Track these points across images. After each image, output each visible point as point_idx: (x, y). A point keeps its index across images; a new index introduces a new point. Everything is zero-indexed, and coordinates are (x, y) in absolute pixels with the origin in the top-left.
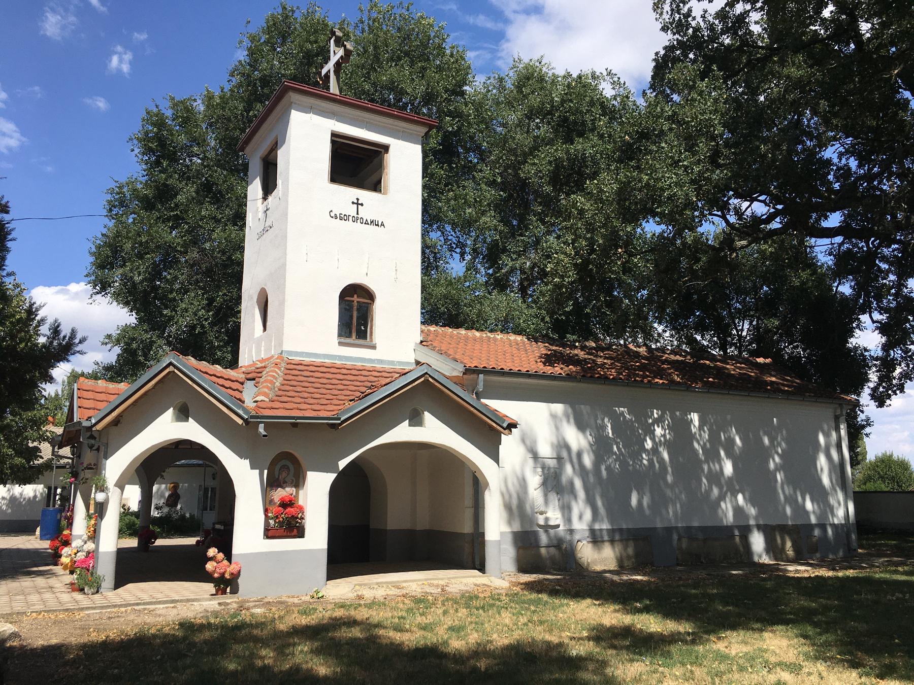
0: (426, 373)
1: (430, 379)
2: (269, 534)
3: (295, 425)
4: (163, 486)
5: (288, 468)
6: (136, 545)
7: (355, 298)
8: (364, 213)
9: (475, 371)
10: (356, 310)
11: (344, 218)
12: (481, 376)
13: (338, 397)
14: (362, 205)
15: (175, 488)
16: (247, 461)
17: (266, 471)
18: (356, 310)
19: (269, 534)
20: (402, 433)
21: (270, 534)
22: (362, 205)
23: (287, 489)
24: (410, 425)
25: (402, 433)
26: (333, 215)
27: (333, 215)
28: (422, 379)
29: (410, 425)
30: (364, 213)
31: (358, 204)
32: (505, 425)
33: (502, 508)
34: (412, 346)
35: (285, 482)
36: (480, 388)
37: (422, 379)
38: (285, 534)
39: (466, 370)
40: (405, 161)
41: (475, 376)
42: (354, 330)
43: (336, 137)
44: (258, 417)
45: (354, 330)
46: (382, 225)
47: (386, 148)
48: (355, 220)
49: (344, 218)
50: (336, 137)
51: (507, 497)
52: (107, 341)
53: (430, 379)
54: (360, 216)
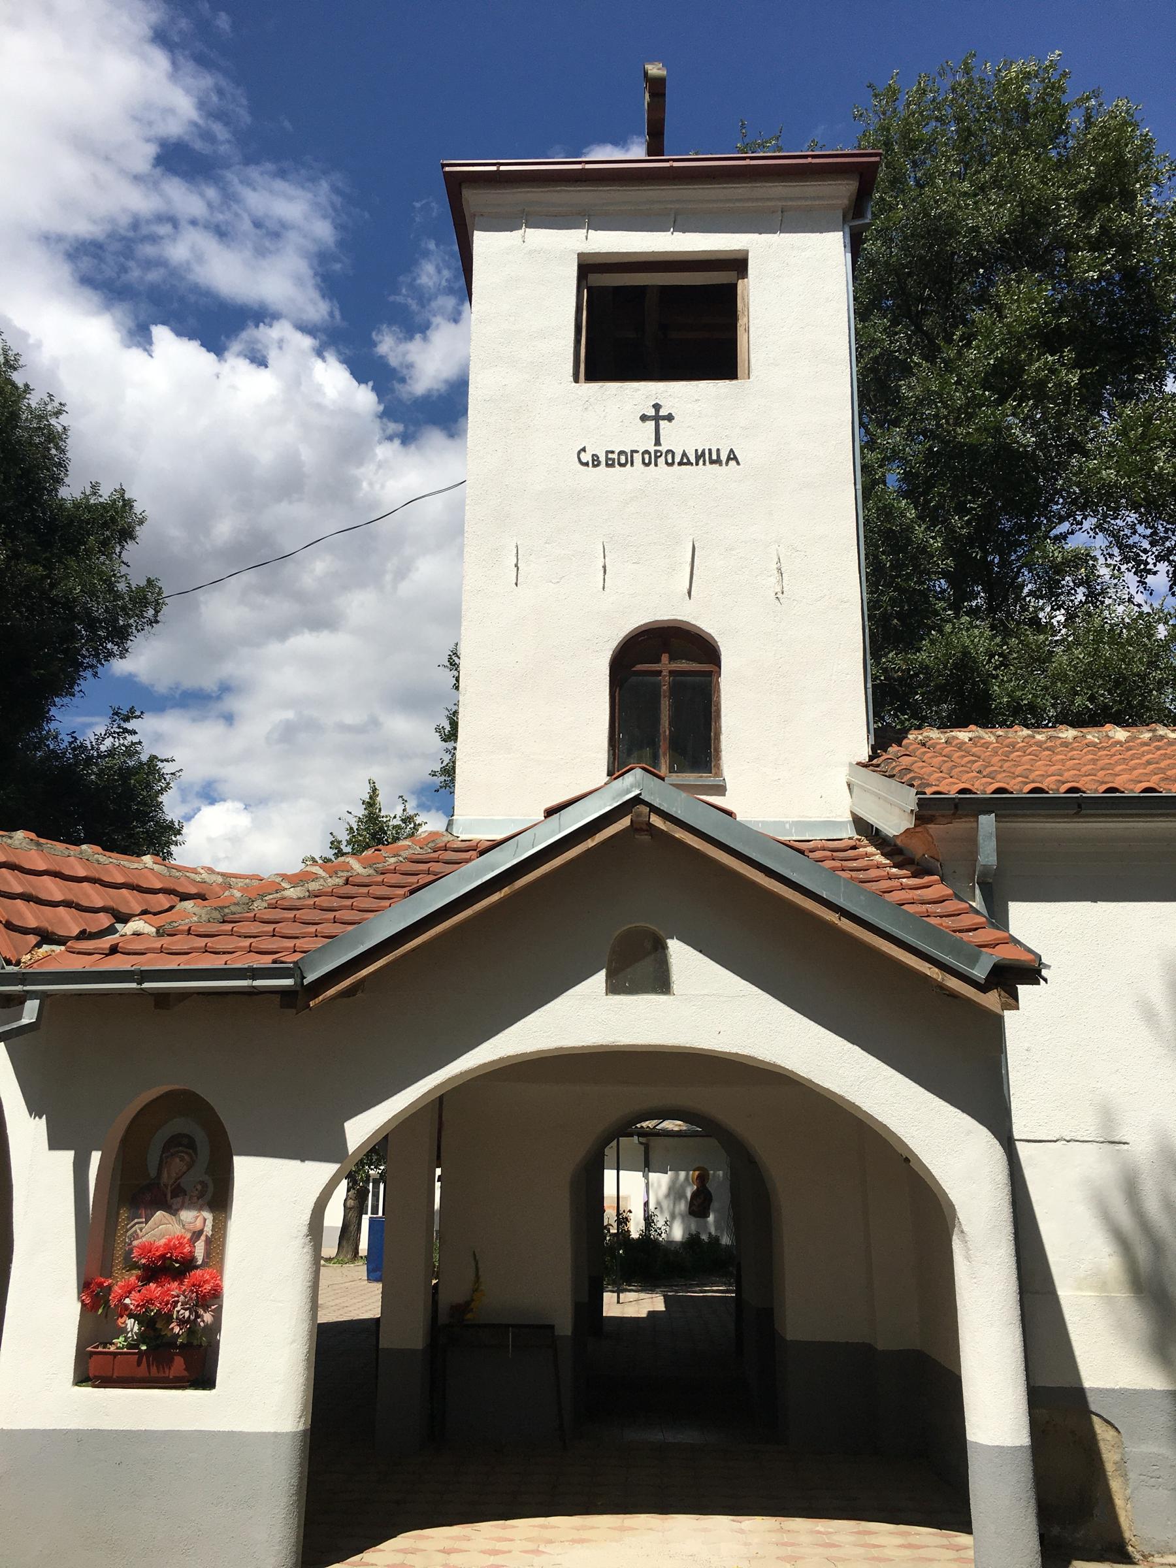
0: (637, 800)
1: (656, 820)
2: (93, 1368)
3: (162, 999)
4: (682, 1174)
5: (191, 1145)
6: (609, 1298)
7: (666, 664)
8: (675, 438)
9: (966, 806)
10: (665, 690)
11: (618, 460)
12: (987, 822)
13: (356, 902)
14: (670, 418)
15: (702, 1179)
16: (42, 1123)
17: (96, 1157)
18: (665, 690)
19: (93, 1368)
20: (585, 1016)
21: (93, 1368)
22: (670, 418)
23: (187, 1215)
24: (613, 988)
25: (585, 1016)
26: (586, 457)
27: (586, 457)
28: (625, 822)
29: (613, 988)
30: (675, 438)
31: (657, 418)
32: (980, 972)
33: (1122, 1295)
34: (841, 776)
35: (178, 1191)
36: (988, 855)
37: (625, 822)
38: (142, 1371)
39: (922, 803)
40: (800, 292)
41: (959, 826)
42: (664, 746)
43: (588, 267)
44: (24, 978)
45: (664, 746)
46: (732, 457)
47: (738, 264)
48: (650, 458)
49: (618, 460)
50: (588, 267)
51: (1142, 1253)
52: (320, 862)
53: (656, 820)
54: (663, 448)
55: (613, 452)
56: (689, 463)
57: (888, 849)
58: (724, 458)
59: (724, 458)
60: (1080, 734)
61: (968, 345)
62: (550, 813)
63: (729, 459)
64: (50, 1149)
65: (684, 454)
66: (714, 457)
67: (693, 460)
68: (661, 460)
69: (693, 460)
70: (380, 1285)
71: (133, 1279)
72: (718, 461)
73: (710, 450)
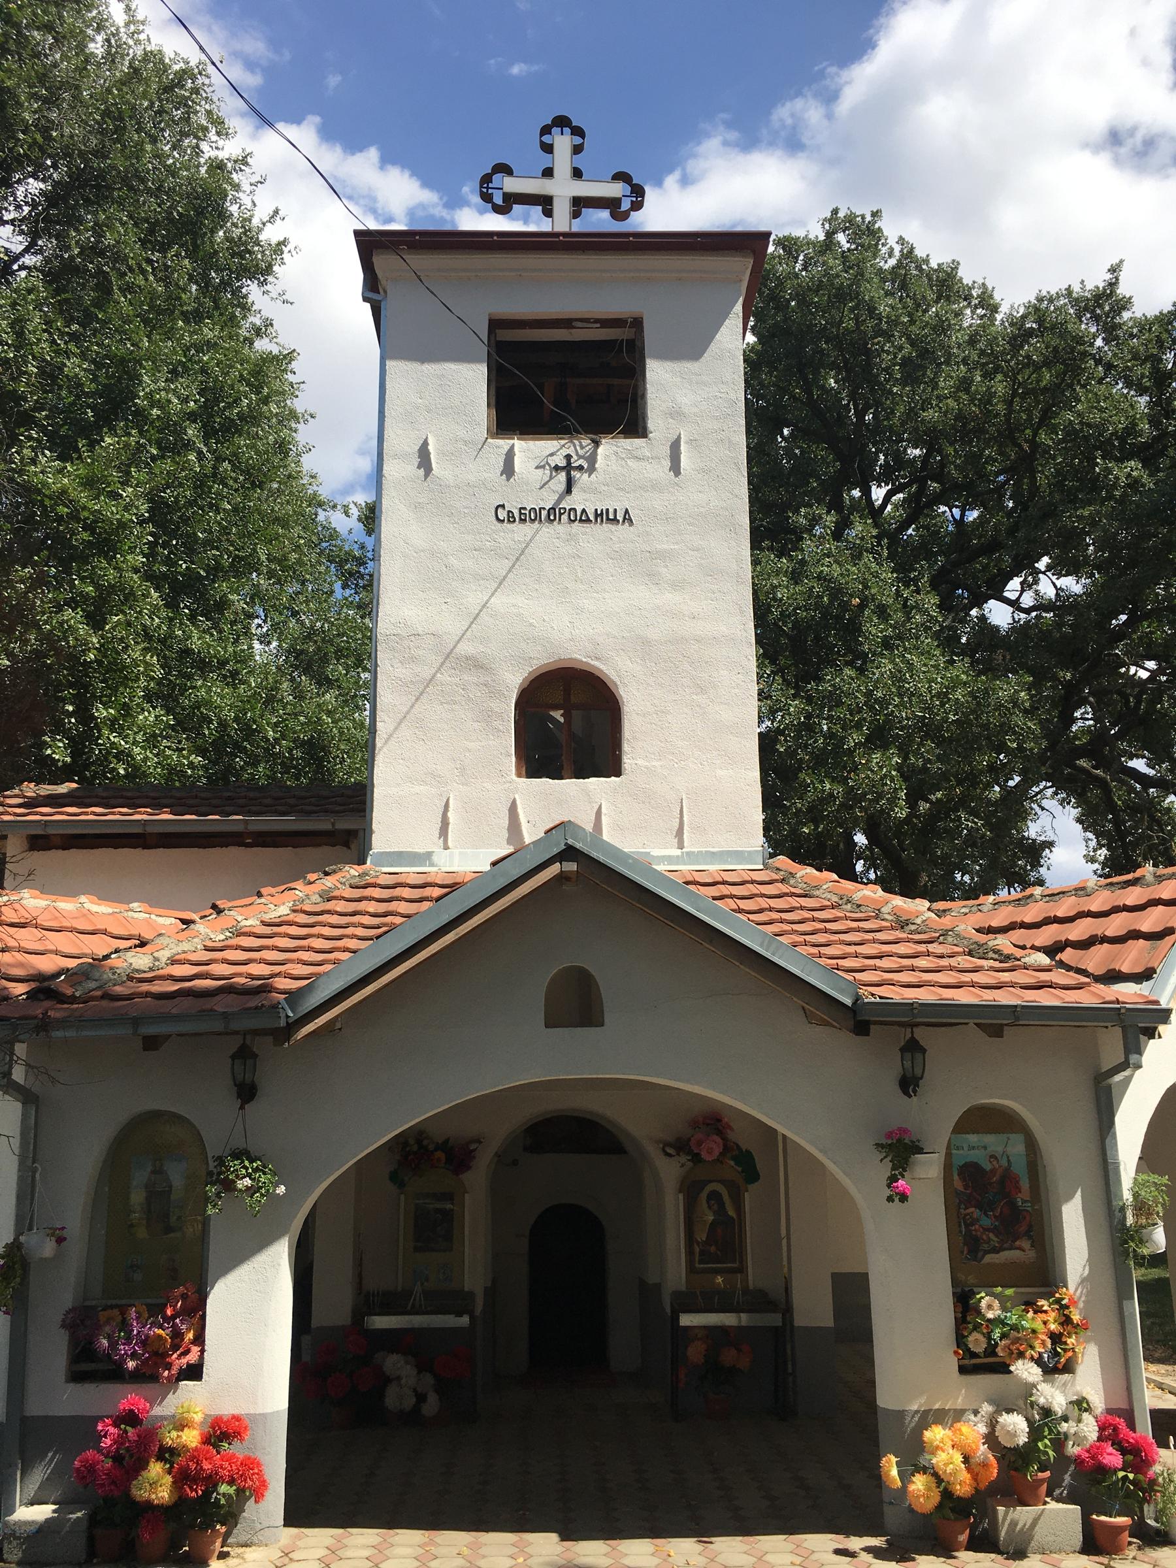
27: (502, 514)
55: (525, 509)
56: (588, 520)
57: (930, 1418)
58: (620, 517)
59: (620, 517)
60: (609, 1549)
61: (882, 404)
62: (494, 864)
63: (625, 518)
64: (618, 773)
65: (584, 511)
66: (611, 517)
67: (592, 518)
68: (565, 517)
69: (592, 518)
70: (830, 1323)
71: (1151, 869)
72: (615, 520)
73: (607, 510)
